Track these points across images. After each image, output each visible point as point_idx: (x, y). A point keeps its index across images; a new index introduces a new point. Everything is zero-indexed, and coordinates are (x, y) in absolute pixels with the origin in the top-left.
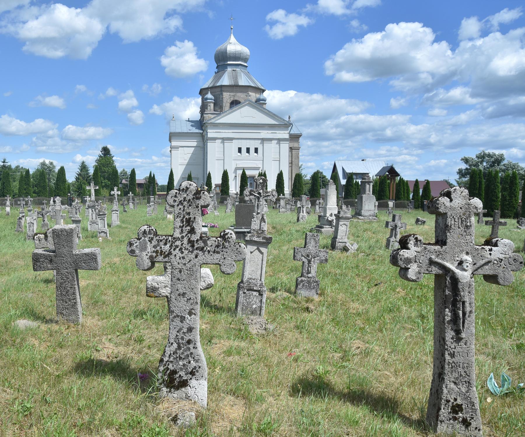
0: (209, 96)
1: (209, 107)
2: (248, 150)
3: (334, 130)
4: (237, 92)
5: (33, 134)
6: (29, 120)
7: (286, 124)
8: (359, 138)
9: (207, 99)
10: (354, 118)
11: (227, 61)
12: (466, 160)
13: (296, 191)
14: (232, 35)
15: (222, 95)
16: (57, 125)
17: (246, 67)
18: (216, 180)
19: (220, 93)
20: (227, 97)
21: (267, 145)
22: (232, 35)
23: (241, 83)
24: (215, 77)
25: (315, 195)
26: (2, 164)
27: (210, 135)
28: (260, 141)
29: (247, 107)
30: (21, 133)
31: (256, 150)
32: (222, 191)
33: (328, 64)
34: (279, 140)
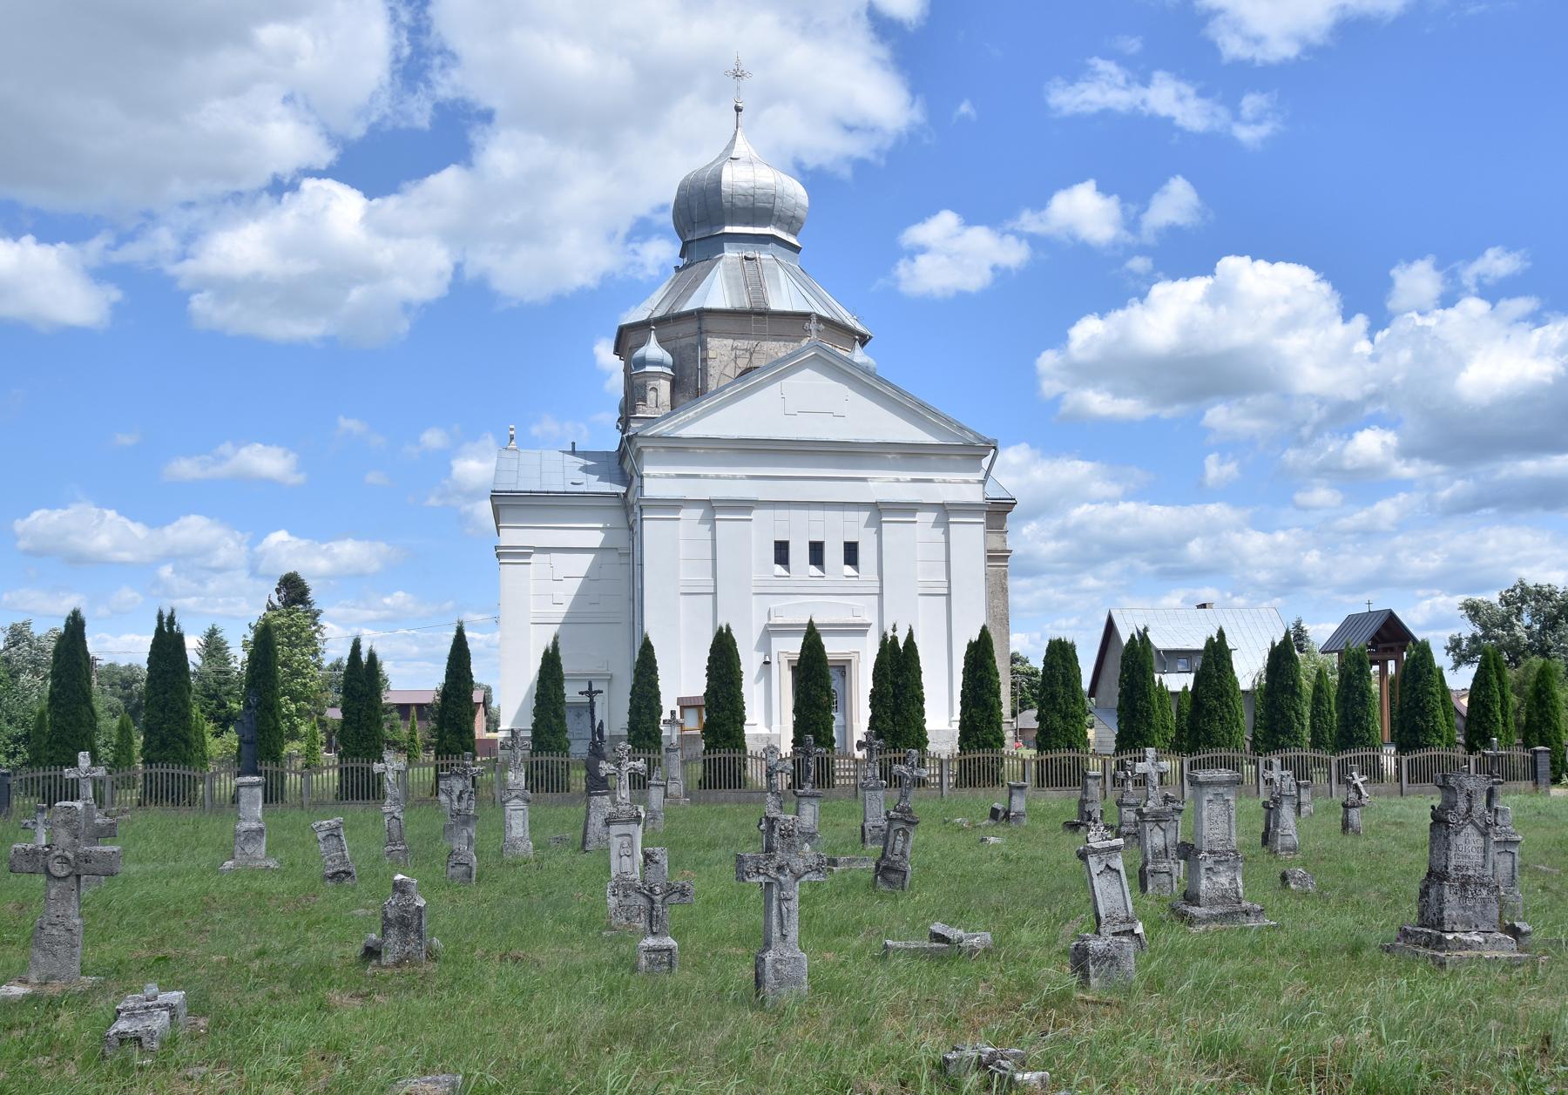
0: (653, 349)
1: (651, 395)
2: (817, 552)
3: (1052, 546)
4: (761, 337)
5: (170, 556)
6: (157, 519)
7: (972, 446)
8: (1113, 567)
9: (643, 362)
10: (1106, 513)
11: (723, 224)
12: (1473, 610)
13: (1058, 722)
15: (704, 349)
17: (796, 249)
18: (682, 679)
19: (694, 340)
20: (721, 351)
21: (893, 531)
23: (776, 305)
24: (675, 284)
28: (865, 515)
29: (807, 373)
31: (851, 553)
32: (708, 729)
33: (1048, 360)
34: (946, 512)
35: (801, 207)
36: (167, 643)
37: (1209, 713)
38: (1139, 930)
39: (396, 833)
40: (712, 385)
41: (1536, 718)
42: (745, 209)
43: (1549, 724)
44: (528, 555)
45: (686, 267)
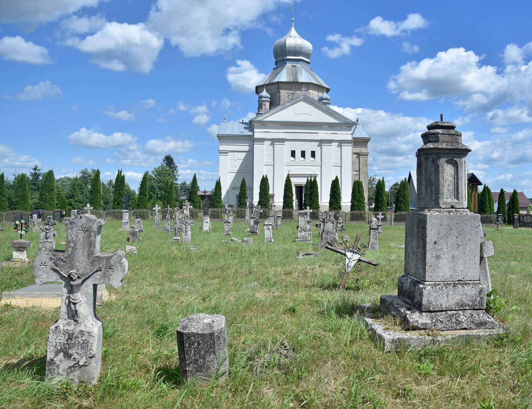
0: (265, 93)
1: (264, 107)
2: (303, 154)
4: (296, 89)
6: (108, 132)
11: (287, 56)
13: (356, 203)
14: (293, 28)
15: (279, 93)
16: (136, 138)
19: (276, 90)
20: (284, 93)
21: (325, 148)
22: (293, 28)
23: (301, 80)
24: (273, 73)
25: (380, 208)
26: (33, 171)
27: (256, 136)
29: (301, 102)
30: (102, 146)
31: (313, 154)
34: (341, 143)
35: (310, 50)
36: (120, 179)
37: (400, 202)
38: (272, 240)
39: (158, 224)
40: (281, 103)
41: (511, 206)
42: (293, 51)
43: (515, 208)
44: (227, 153)
45: (276, 68)
